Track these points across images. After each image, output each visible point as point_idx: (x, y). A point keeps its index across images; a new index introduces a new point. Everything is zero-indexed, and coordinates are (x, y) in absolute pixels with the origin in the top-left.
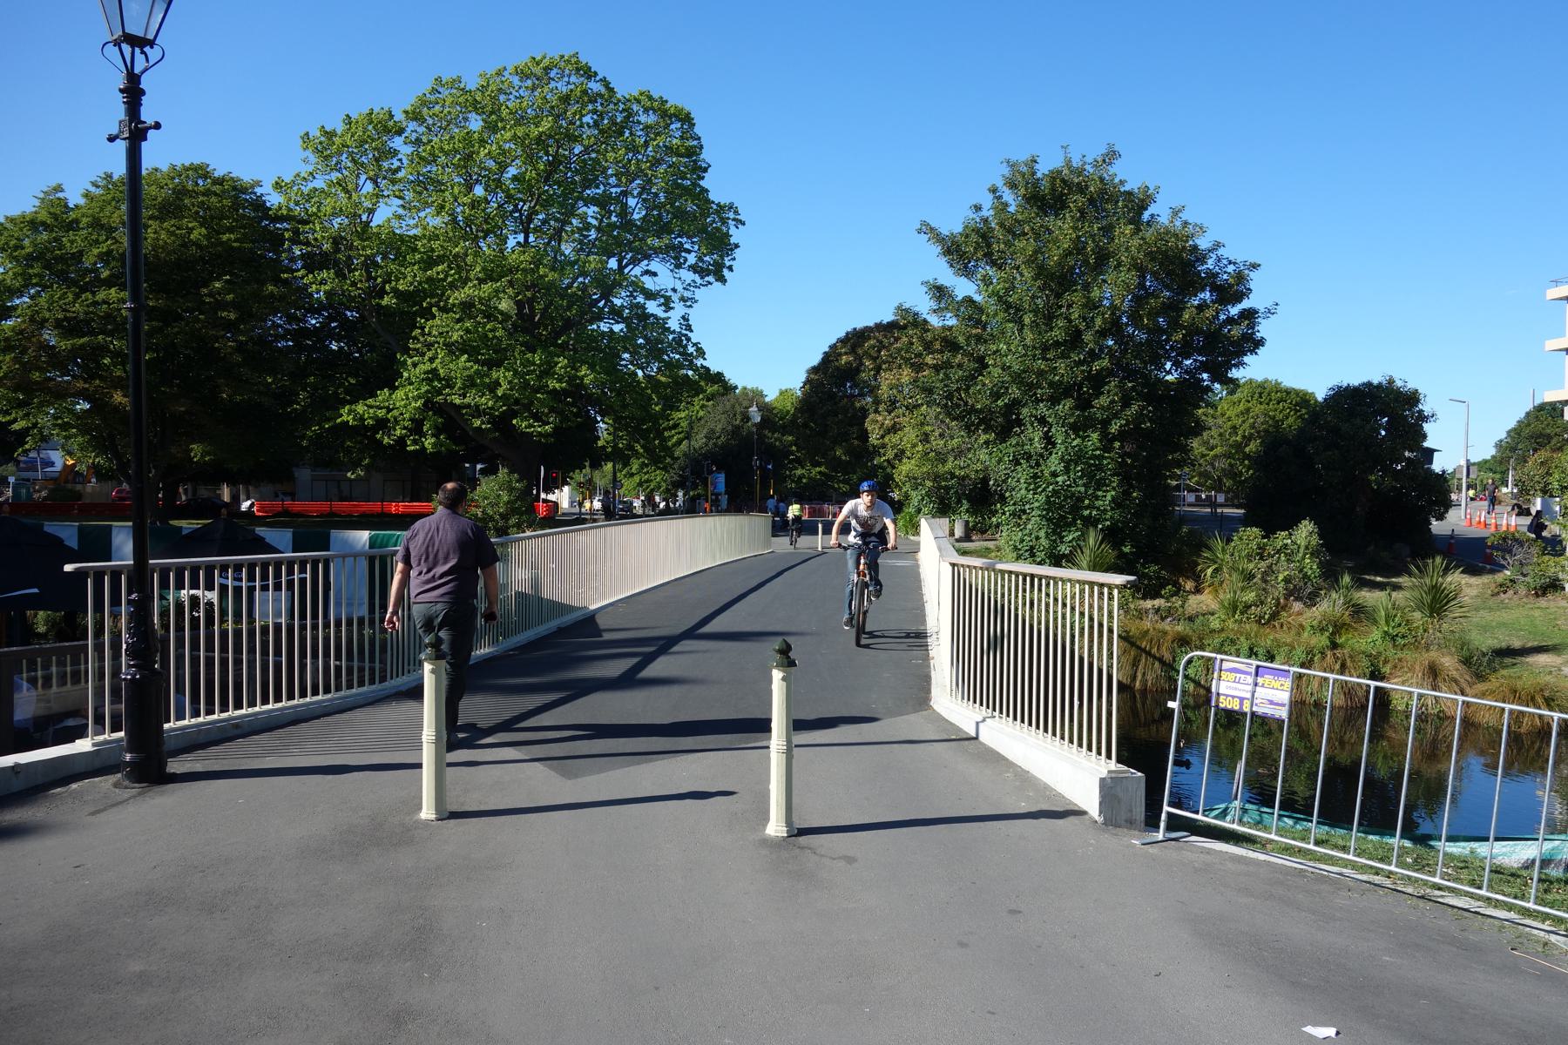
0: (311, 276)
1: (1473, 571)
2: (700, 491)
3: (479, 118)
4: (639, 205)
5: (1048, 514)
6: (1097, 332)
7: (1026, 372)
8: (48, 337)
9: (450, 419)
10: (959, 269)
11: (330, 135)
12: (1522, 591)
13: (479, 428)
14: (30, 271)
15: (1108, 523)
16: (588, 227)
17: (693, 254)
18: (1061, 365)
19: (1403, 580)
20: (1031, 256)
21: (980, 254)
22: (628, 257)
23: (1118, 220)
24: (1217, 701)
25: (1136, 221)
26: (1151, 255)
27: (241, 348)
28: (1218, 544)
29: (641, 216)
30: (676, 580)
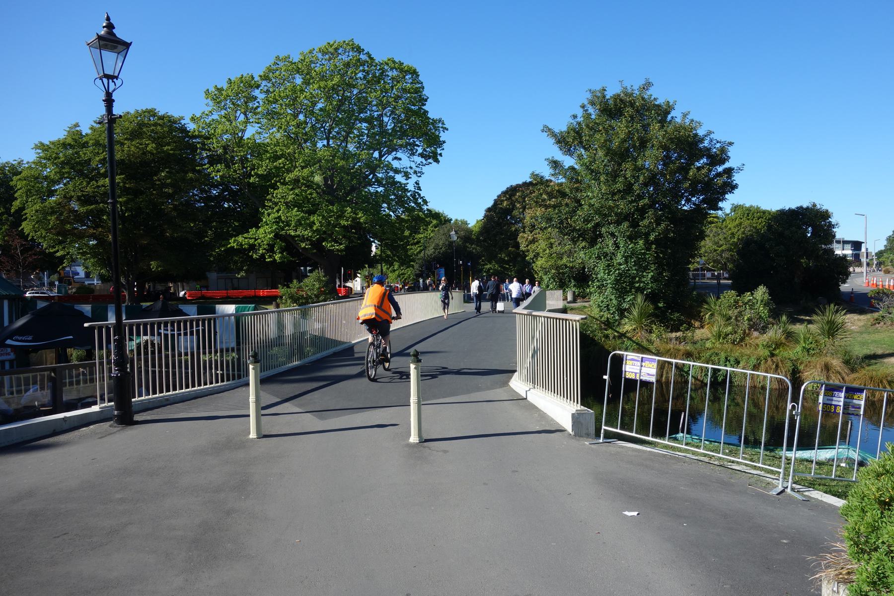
3: (300, 77)
5: (615, 286)
6: (641, 184)
7: (602, 208)
8: (73, 206)
9: (289, 244)
10: (565, 151)
11: (220, 90)
13: (304, 248)
15: (650, 290)
16: (362, 134)
17: (421, 147)
18: (622, 204)
19: (815, 317)
20: (603, 143)
22: (384, 150)
23: (652, 121)
24: (625, 375)
25: (663, 122)
27: (175, 208)
28: (712, 299)
29: (391, 127)
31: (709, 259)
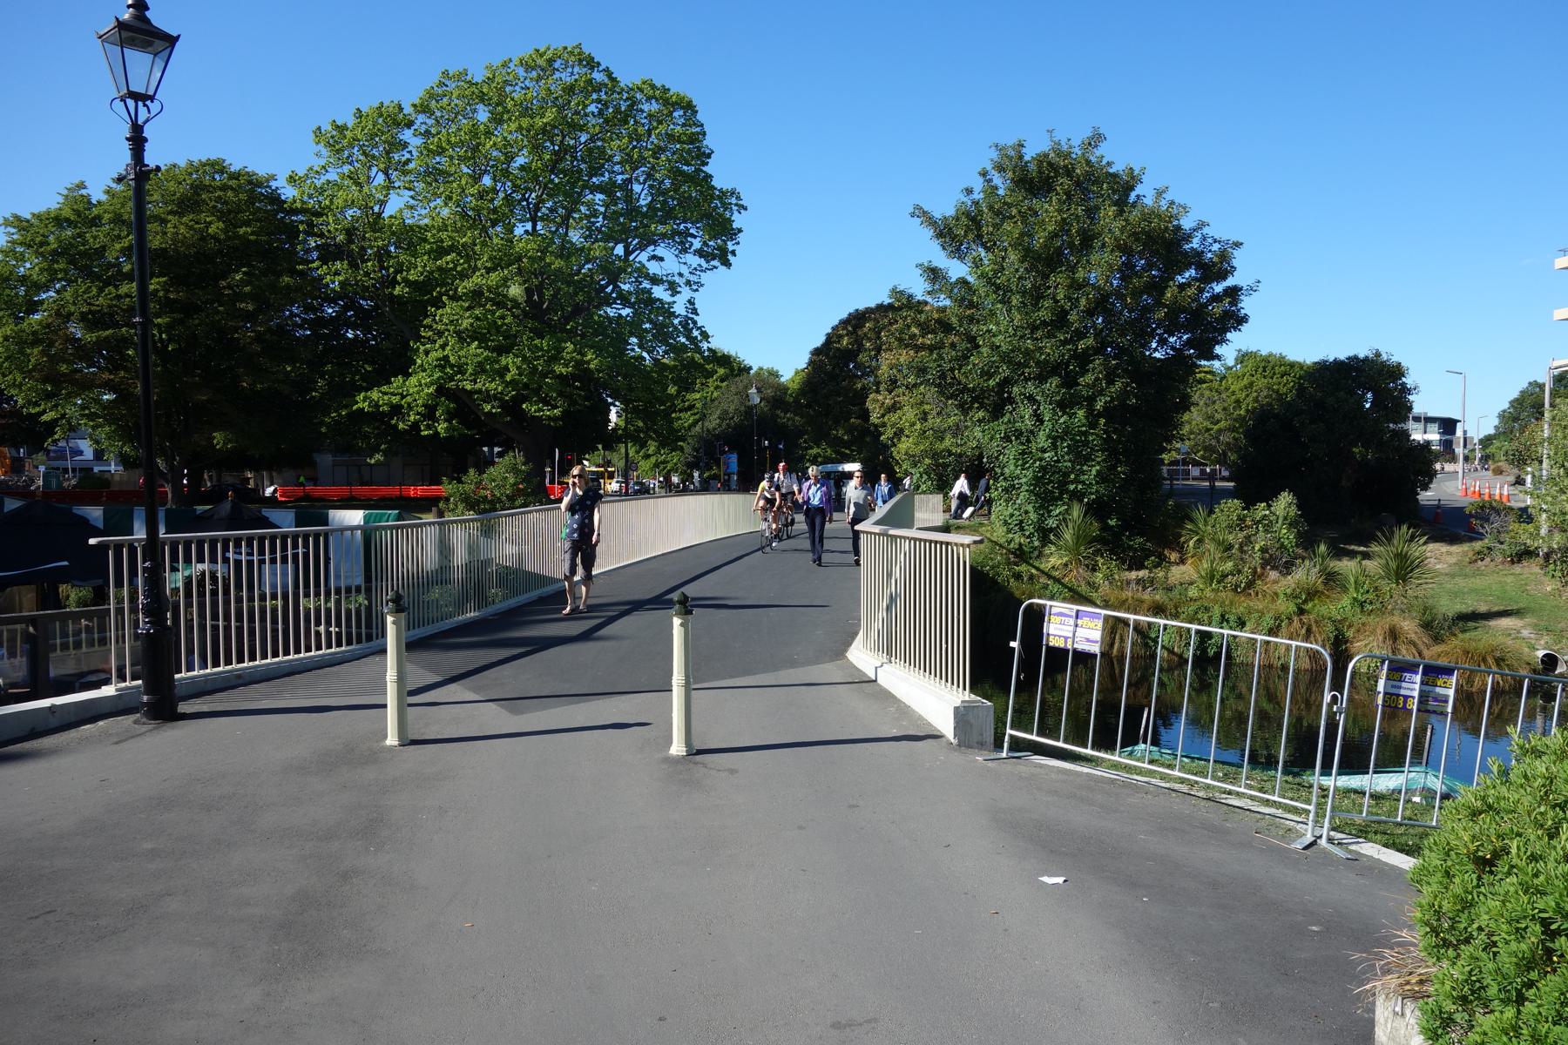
0: (325, 267)
1: (1453, 540)
2: (715, 471)
3: (486, 109)
4: (645, 192)
5: (1035, 489)
6: (1083, 312)
9: (462, 405)
11: (341, 129)
12: (1499, 559)
13: (490, 413)
14: (56, 266)
16: (595, 214)
17: (699, 239)
18: (1048, 346)
19: (1375, 548)
20: (1018, 239)
21: (971, 236)
24: (1048, 640)
25: (1122, 204)
26: (1135, 235)
27: (259, 338)
28: (1200, 514)
30: (663, 555)
31: (1196, 445)
